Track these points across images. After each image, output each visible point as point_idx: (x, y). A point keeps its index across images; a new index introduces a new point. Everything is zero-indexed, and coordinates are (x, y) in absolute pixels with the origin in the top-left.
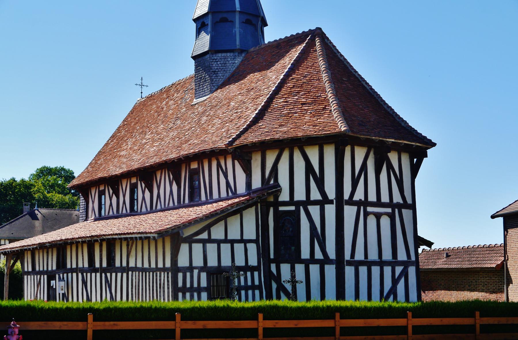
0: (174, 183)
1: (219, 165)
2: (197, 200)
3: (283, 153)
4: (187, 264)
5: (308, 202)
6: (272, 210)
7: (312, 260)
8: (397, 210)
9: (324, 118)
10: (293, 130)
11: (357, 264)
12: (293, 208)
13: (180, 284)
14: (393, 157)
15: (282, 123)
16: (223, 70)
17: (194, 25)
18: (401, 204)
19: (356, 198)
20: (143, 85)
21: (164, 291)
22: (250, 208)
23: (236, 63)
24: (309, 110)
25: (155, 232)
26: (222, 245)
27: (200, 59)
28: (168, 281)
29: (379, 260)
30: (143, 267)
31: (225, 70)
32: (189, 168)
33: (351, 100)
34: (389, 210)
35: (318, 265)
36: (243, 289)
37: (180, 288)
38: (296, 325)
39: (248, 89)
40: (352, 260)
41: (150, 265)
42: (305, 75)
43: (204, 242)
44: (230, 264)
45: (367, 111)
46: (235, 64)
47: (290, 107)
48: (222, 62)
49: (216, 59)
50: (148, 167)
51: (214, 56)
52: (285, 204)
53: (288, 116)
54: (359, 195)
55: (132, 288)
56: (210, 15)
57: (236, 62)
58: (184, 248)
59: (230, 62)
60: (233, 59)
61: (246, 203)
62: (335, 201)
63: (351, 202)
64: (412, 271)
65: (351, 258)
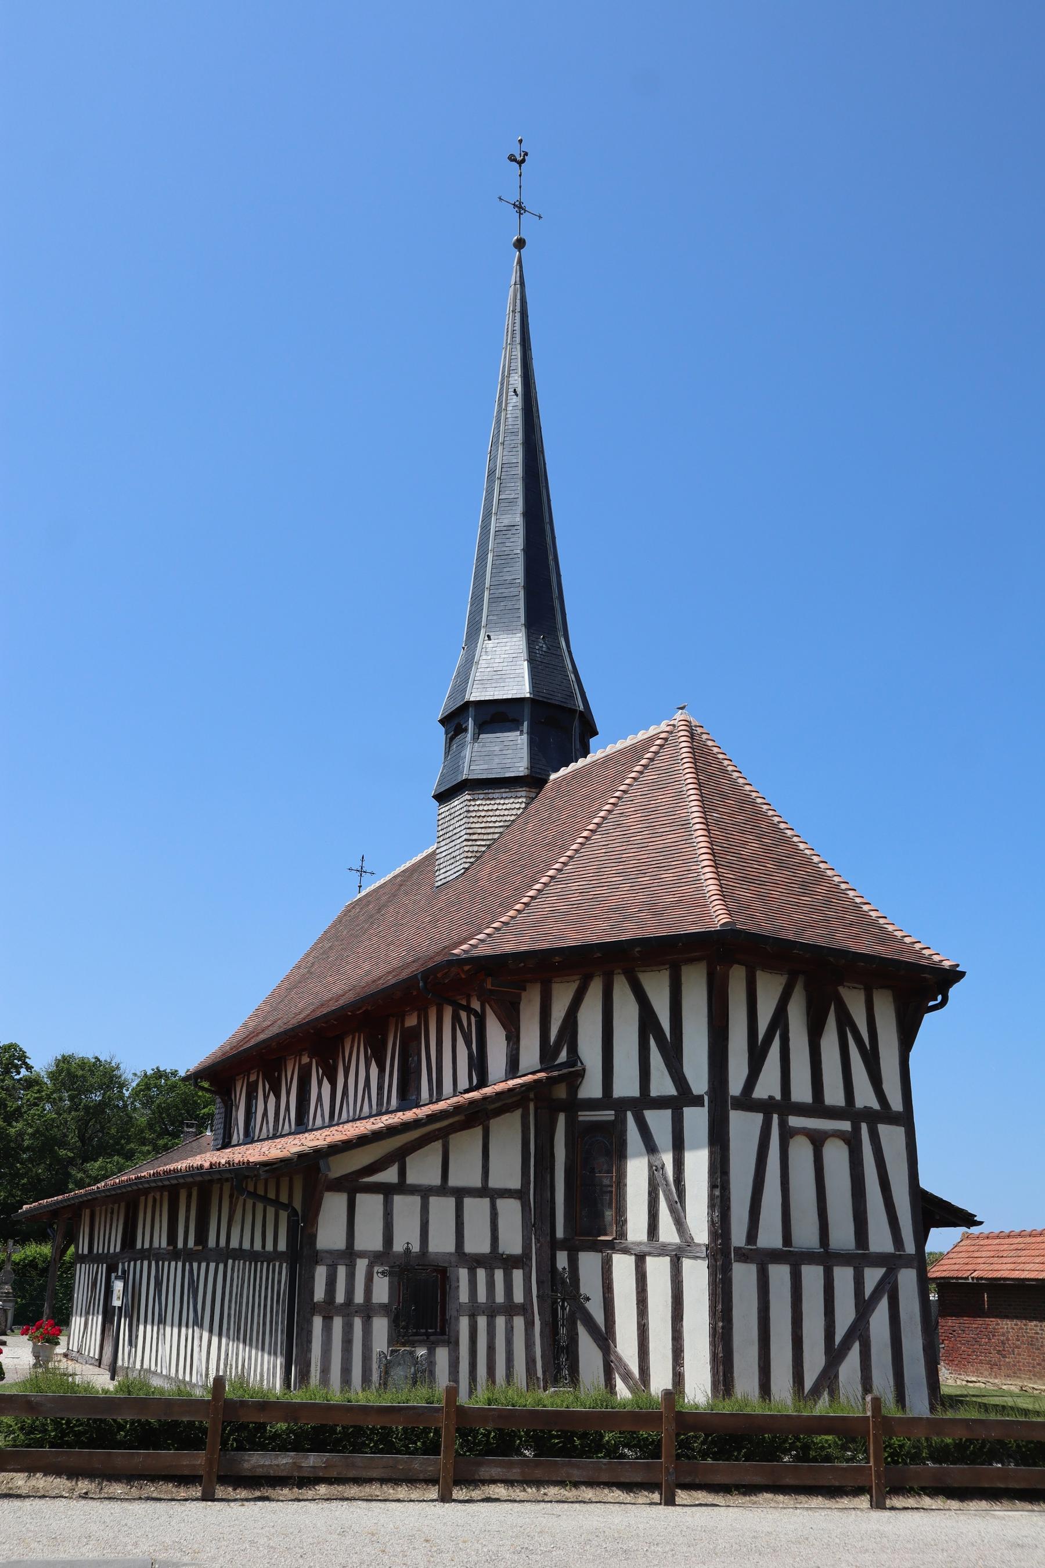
0: (373, 1063)
3: (589, 985)
4: (340, 1244)
5: (645, 1101)
6: (562, 1119)
8: (864, 1127)
11: (763, 1259)
12: (608, 1115)
18: (876, 1111)
19: (761, 1092)
20: (358, 871)
29: (822, 1250)
34: (846, 1126)
40: (749, 1247)
41: (264, 1246)
54: (768, 1086)
56: (470, 709)
58: (334, 1205)
62: (706, 1098)
63: (746, 1102)
64: (907, 1279)
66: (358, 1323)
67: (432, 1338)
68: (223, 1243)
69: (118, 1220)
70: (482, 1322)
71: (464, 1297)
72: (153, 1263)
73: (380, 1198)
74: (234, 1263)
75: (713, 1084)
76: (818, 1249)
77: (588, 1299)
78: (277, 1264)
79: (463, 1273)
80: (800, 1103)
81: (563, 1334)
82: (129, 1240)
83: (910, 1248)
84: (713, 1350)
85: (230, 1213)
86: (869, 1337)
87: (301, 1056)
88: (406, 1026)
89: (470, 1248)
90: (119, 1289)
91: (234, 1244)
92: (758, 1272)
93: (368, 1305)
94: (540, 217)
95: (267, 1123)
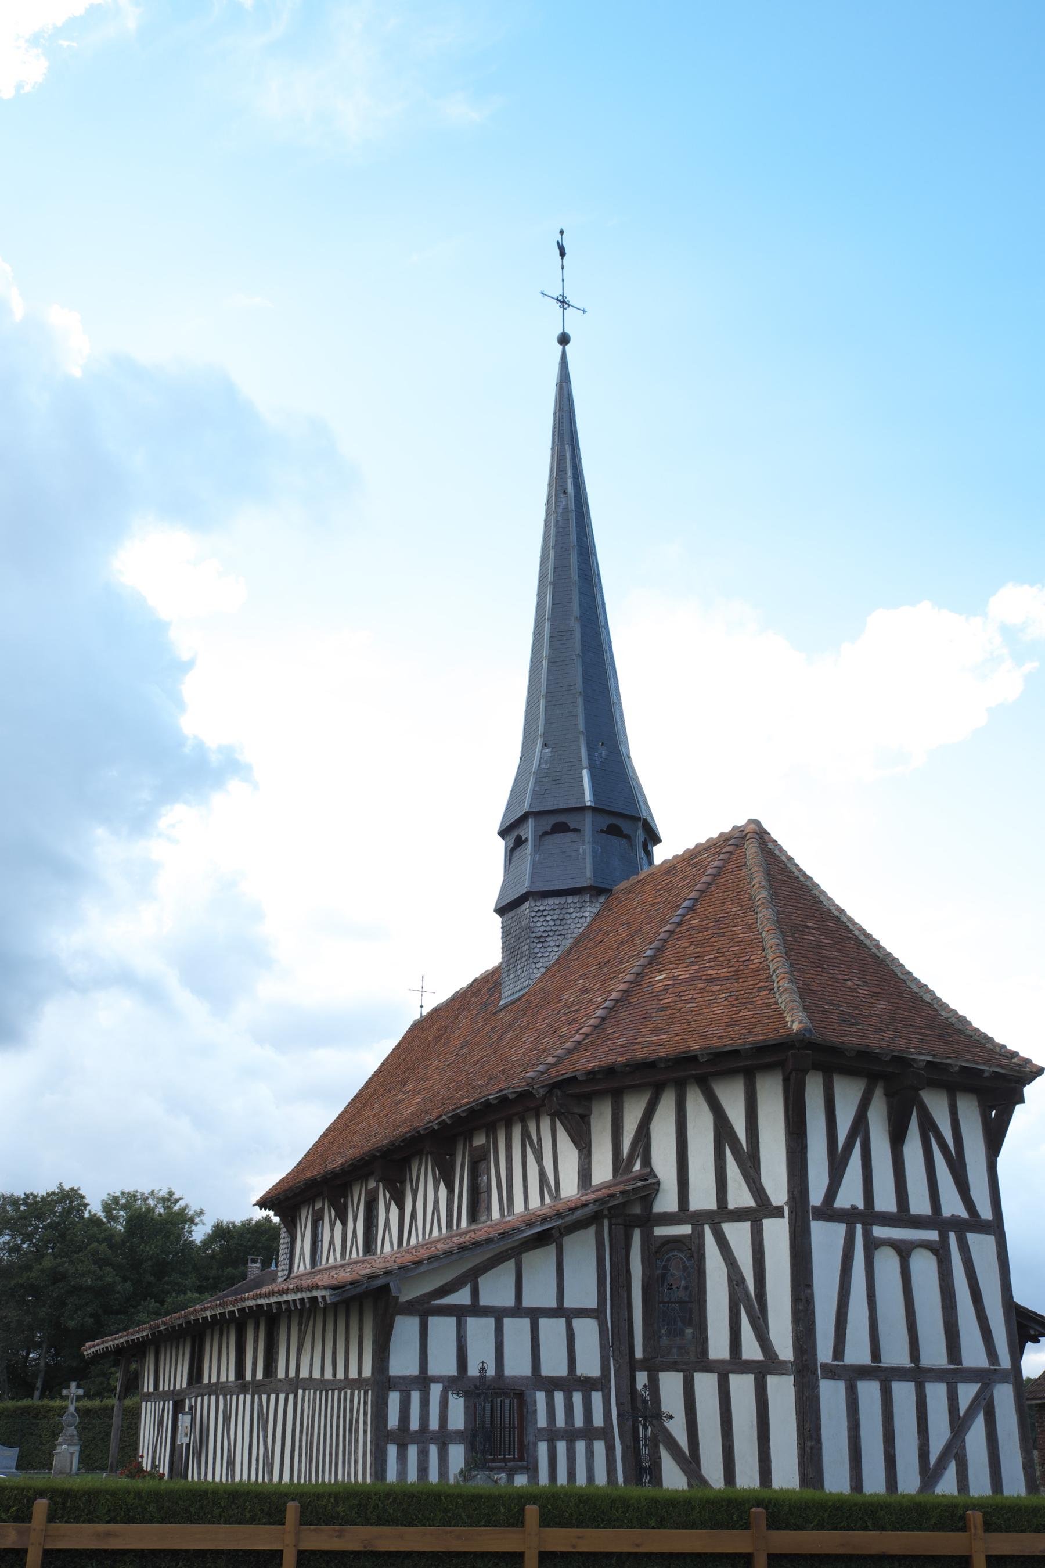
0: (442, 1185)
1: (526, 1136)
2: (484, 1218)
4: (414, 1370)
5: (723, 1213)
7: (737, 1363)
8: (952, 1236)
9: (755, 1008)
10: (680, 1038)
12: (686, 1230)
13: (393, 1421)
14: (938, 1106)
15: (660, 1025)
16: (557, 933)
17: (501, 843)
18: (965, 1220)
21: (357, 1441)
22: (581, 1231)
23: (586, 917)
24: (723, 994)
25: (326, 1288)
26: (507, 1321)
27: (511, 914)
28: (365, 1414)
29: (913, 1365)
30: (323, 1377)
31: (563, 932)
32: (469, 1146)
33: (825, 968)
34: (933, 1235)
35: (751, 1377)
36: (563, 1437)
37: (391, 1432)
38: (638, 1545)
39: (599, 964)
40: (836, 1363)
41: (335, 1375)
42: (717, 919)
43: (460, 1313)
44: (526, 1370)
45: (863, 994)
46: (583, 920)
47: (679, 990)
48: (555, 917)
49: (543, 911)
50: (389, 1149)
51: (539, 904)
52: (668, 1219)
53: (674, 1009)
54: (850, 1196)
55: (301, 1432)
57: (587, 914)
58: (406, 1328)
59: (574, 915)
60: (580, 908)
61: (568, 1215)
62: (786, 1209)
63: (828, 1213)
65: (835, 1358)
66: (433, 1450)
67: (510, 1464)
68: (292, 1374)
69: (183, 1355)
70: (561, 1447)
71: (542, 1422)
72: (221, 1397)
73: (453, 1320)
74: (304, 1393)
75: (793, 1194)
76: (908, 1364)
77: (671, 1417)
78: (349, 1392)
79: (541, 1397)
80: (884, 1212)
81: (645, 1454)
82: (195, 1375)
83: (1005, 1362)
84: (803, 1471)
85: (299, 1342)
86: (965, 1456)
87: (367, 1181)
88: (474, 1146)
89: (546, 1371)
90: (186, 1425)
91: (304, 1373)
92: (847, 1389)
93: (443, 1432)
94: (584, 311)
95: (334, 1250)
